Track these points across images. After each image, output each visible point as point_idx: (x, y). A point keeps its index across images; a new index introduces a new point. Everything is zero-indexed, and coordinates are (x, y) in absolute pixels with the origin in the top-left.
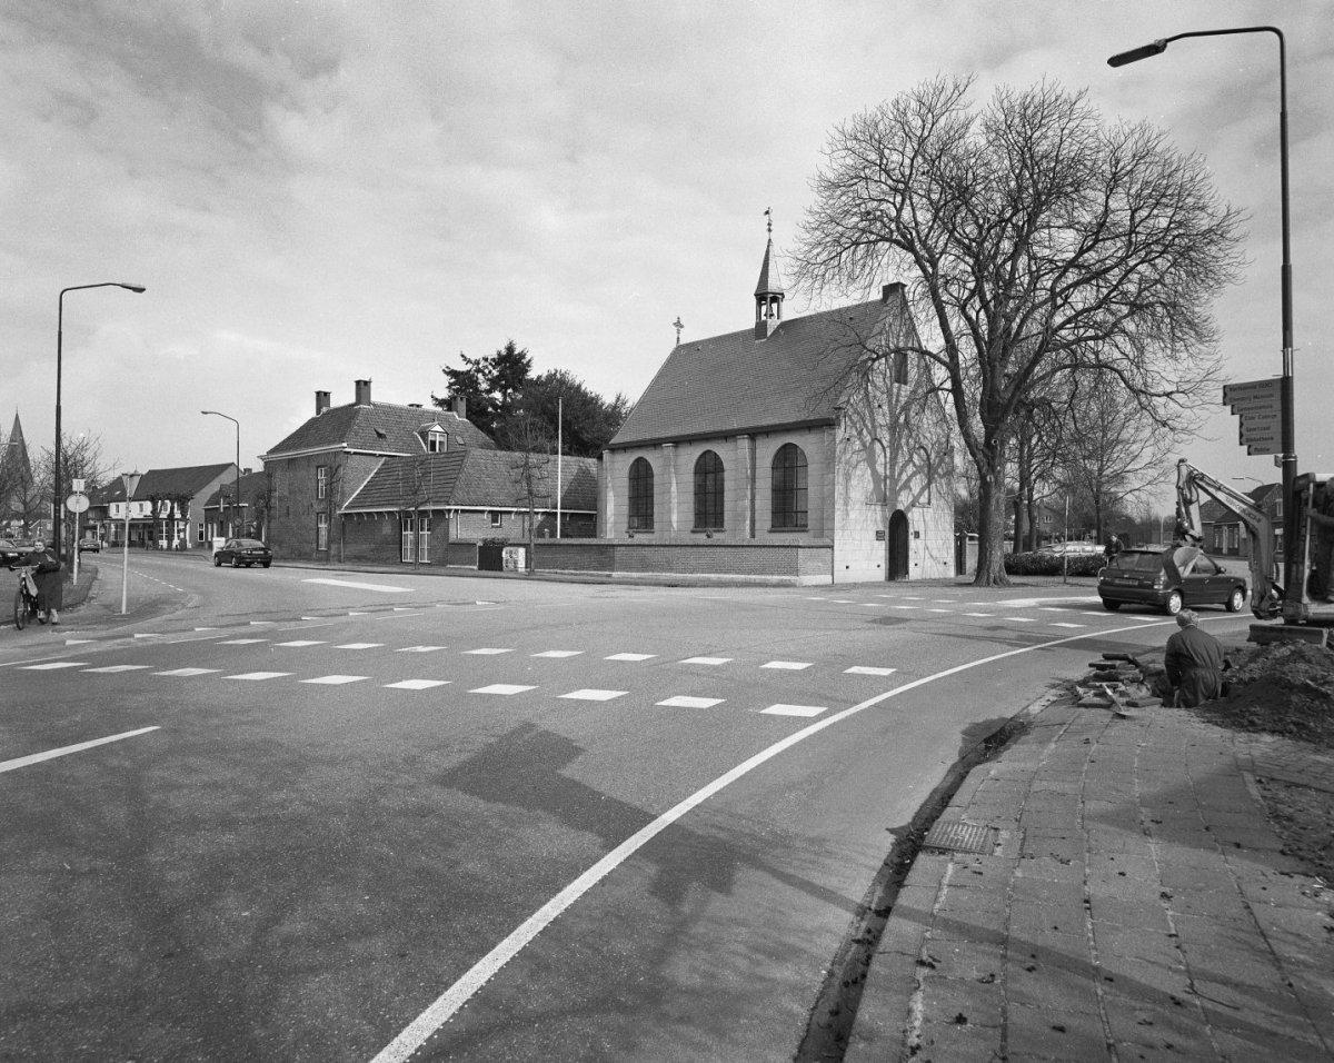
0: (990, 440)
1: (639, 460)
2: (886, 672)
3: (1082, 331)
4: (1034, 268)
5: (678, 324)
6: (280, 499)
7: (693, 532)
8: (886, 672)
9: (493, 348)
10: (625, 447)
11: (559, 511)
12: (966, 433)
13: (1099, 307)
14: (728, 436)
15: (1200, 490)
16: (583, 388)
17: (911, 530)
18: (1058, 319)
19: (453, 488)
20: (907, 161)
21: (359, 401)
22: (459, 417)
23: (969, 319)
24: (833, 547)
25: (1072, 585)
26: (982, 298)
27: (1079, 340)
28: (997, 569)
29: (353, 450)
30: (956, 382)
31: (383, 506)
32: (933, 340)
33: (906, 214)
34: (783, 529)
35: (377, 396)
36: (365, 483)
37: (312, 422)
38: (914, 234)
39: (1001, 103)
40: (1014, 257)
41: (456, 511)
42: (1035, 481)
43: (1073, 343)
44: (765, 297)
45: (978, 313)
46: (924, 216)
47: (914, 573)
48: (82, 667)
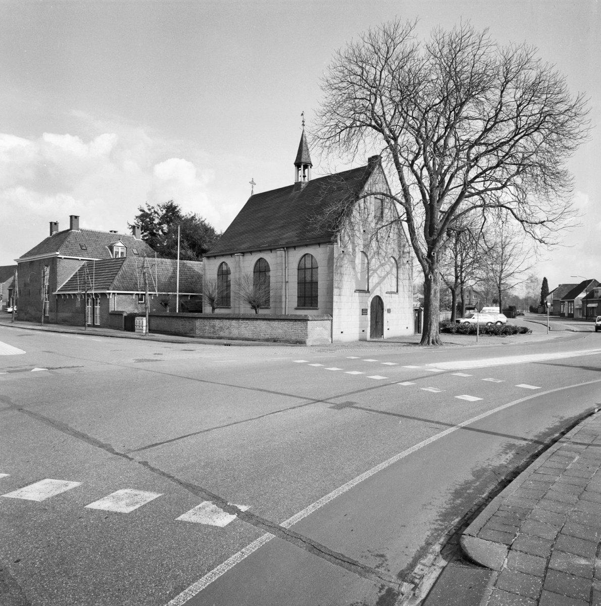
0: (431, 252)
1: (260, 260)
3: (488, 183)
5: (252, 183)
7: (296, 309)
9: (164, 200)
11: (178, 293)
12: (417, 250)
15: (450, 187)
16: (178, 208)
18: (472, 174)
19: (113, 279)
20: (378, 73)
21: (71, 229)
23: (414, 171)
28: (435, 335)
29: (63, 257)
30: (409, 213)
32: (396, 189)
34: (304, 307)
35: (83, 225)
37: (48, 239)
38: (383, 120)
39: (436, 36)
41: (114, 294)
43: (482, 192)
44: (301, 163)
46: (390, 110)
47: (387, 334)
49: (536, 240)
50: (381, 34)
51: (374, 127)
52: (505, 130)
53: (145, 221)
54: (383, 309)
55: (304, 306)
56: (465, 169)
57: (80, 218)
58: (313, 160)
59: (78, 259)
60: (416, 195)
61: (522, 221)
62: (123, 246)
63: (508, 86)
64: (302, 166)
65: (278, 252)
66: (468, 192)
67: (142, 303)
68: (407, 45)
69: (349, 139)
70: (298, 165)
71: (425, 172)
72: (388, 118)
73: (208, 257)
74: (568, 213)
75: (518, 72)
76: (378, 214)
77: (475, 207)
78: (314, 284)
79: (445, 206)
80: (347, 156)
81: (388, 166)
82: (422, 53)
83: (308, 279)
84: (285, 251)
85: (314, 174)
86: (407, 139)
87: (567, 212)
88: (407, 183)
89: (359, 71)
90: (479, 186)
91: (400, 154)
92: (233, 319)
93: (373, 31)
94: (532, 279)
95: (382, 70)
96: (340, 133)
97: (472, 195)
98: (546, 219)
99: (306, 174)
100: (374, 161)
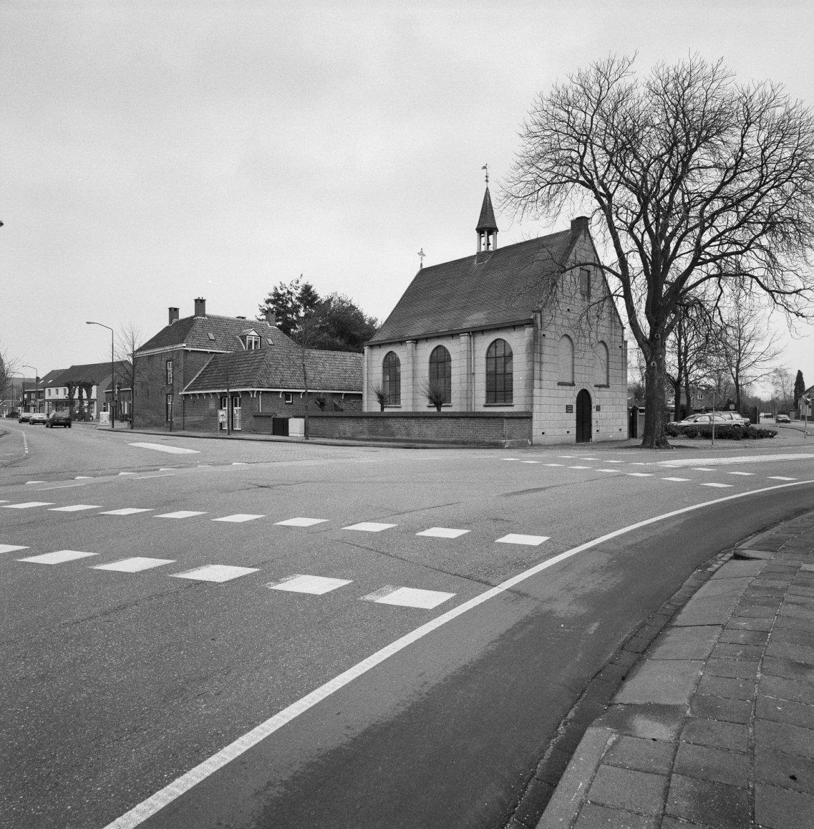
1: (439, 347)
2: (536, 540)
3: (726, 246)
4: (687, 201)
5: (422, 254)
6: (143, 384)
7: (485, 406)
8: (536, 540)
10: (380, 345)
13: (738, 226)
14: (453, 335)
15: (678, 253)
16: (312, 289)
17: (593, 405)
18: (706, 237)
20: (589, 118)
22: (272, 326)
23: (634, 237)
24: (530, 418)
25: (719, 448)
26: (646, 221)
27: (724, 255)
29: (190, 349)
31: (208, 389)
32: (608, 256)
33: (588, 159)
34: (494, 404)
35: (210, 310)
36: (200, 372)
38: (594, 176)
40: (672, 191)
42: (691, 367)
44: (487, 227)
45: (643, 235)
46: (602, 159)
47: (595, 436)
48: (49, 507)
49: (790, 314)
50: (593, 71)
51: (582, 183)
52: (749, 178)
53: (279, 306)
54: (591, 406)
55: (496, 402)
56: (697, 231)
57: (206, 302)
58: (499, 223)
59: (206, 352)
60: (635, 262)
61: (770, 292)
62: (257, 335)
63: (750, 129)
64: (486, 233)
65: (462, 338)
66: (702, 259)
67: (289, 404)
68: (624, 83)
69: (550, 198)
70: (480, 231)
71: (647, 237)
72: (601, 173)
73: (371, 347)
74: (141, 469)
75: (762, 112)
76: (585, 288)
77: (709, 277)
78: (508, 377)
79: (672, 276)
80: (543, 221)
81: (598, 230)
82: (641, 91)
83: (500, 370)
84: (470, 336)
85: (503, 240)
86: (623, 195)
87: (634, 175)
88: (625, 250)
89: (564, 115)
90: (713, 250)
91: (617, 216)
92: (412, 418)
93: (583, 71)
94: (780, 373)
95: (593, 115)
96: (539, 190)
97: (705, 262)
98: (802, 287)
99: (491, 242)
100: (581, 224)
